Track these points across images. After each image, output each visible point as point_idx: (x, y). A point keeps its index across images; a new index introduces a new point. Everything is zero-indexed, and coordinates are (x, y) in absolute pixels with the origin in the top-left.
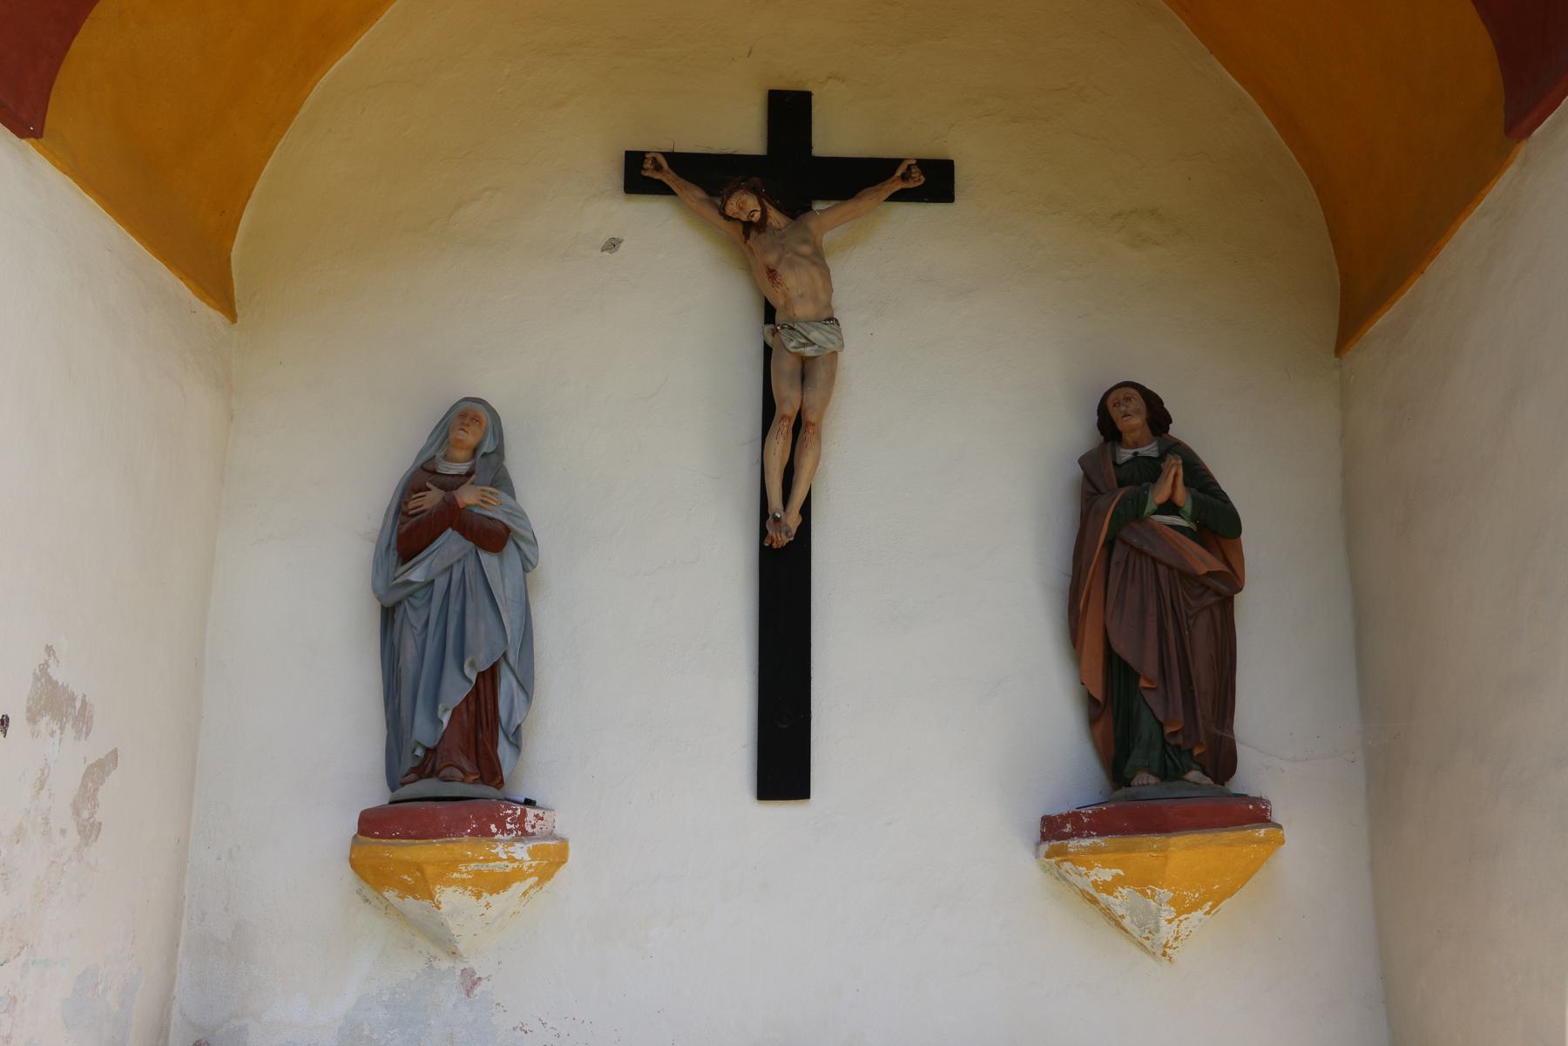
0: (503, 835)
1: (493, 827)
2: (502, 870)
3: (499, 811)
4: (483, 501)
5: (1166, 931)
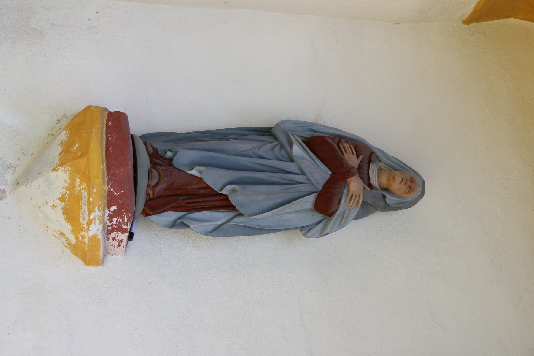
0: (108, 216)
1: (114, 208)
2: (81, 216)
3: (127, 212)
4: (352, 195)
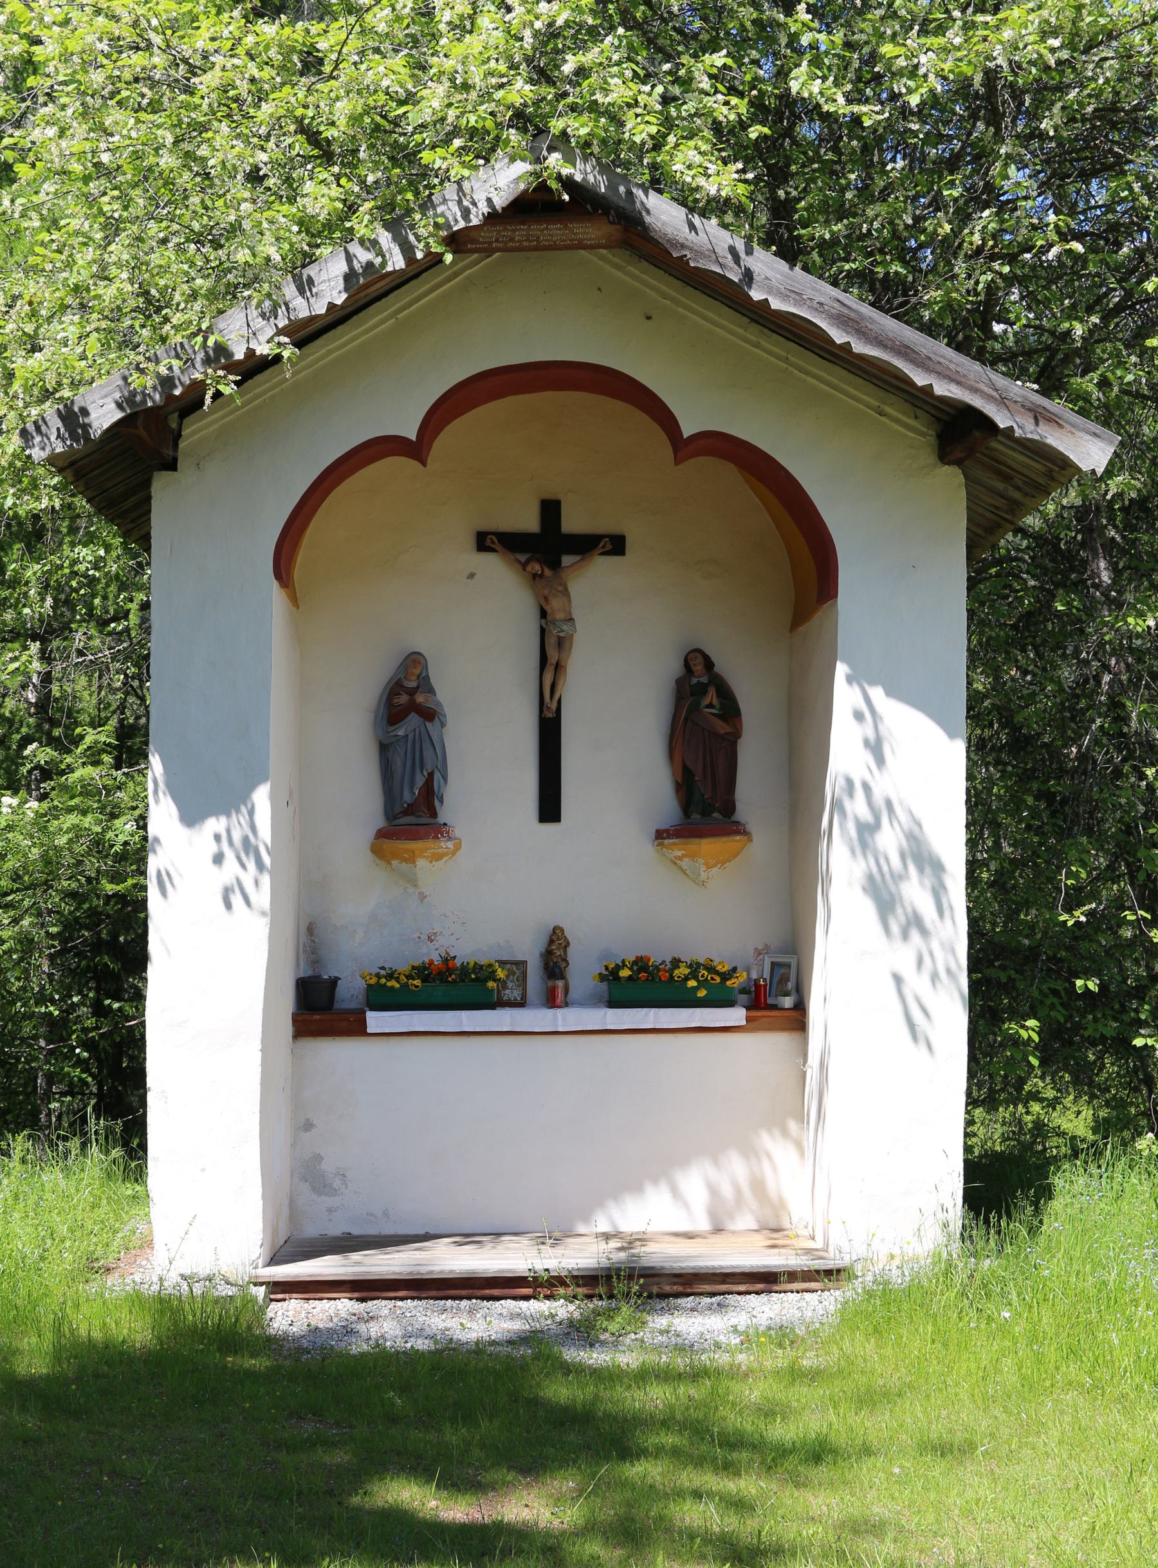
5: (703, 876)
